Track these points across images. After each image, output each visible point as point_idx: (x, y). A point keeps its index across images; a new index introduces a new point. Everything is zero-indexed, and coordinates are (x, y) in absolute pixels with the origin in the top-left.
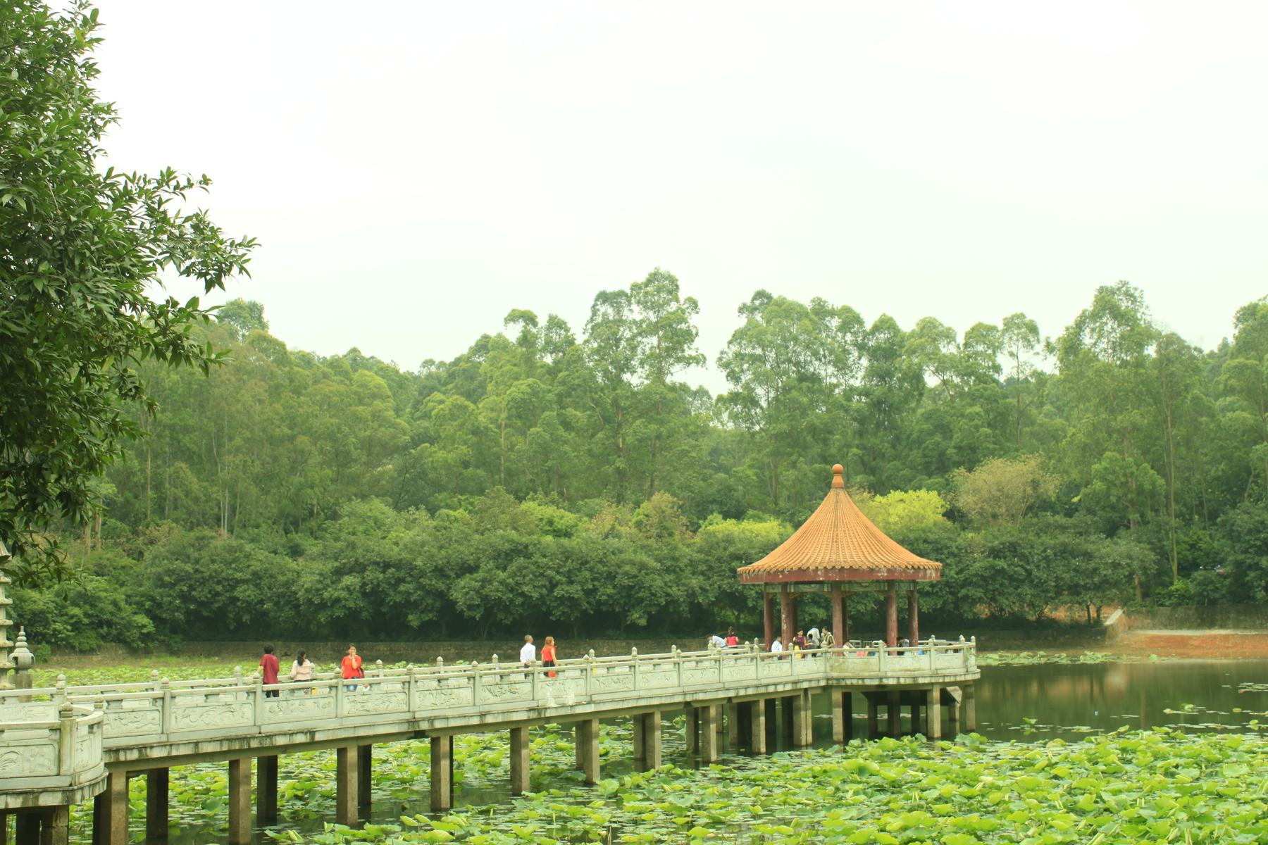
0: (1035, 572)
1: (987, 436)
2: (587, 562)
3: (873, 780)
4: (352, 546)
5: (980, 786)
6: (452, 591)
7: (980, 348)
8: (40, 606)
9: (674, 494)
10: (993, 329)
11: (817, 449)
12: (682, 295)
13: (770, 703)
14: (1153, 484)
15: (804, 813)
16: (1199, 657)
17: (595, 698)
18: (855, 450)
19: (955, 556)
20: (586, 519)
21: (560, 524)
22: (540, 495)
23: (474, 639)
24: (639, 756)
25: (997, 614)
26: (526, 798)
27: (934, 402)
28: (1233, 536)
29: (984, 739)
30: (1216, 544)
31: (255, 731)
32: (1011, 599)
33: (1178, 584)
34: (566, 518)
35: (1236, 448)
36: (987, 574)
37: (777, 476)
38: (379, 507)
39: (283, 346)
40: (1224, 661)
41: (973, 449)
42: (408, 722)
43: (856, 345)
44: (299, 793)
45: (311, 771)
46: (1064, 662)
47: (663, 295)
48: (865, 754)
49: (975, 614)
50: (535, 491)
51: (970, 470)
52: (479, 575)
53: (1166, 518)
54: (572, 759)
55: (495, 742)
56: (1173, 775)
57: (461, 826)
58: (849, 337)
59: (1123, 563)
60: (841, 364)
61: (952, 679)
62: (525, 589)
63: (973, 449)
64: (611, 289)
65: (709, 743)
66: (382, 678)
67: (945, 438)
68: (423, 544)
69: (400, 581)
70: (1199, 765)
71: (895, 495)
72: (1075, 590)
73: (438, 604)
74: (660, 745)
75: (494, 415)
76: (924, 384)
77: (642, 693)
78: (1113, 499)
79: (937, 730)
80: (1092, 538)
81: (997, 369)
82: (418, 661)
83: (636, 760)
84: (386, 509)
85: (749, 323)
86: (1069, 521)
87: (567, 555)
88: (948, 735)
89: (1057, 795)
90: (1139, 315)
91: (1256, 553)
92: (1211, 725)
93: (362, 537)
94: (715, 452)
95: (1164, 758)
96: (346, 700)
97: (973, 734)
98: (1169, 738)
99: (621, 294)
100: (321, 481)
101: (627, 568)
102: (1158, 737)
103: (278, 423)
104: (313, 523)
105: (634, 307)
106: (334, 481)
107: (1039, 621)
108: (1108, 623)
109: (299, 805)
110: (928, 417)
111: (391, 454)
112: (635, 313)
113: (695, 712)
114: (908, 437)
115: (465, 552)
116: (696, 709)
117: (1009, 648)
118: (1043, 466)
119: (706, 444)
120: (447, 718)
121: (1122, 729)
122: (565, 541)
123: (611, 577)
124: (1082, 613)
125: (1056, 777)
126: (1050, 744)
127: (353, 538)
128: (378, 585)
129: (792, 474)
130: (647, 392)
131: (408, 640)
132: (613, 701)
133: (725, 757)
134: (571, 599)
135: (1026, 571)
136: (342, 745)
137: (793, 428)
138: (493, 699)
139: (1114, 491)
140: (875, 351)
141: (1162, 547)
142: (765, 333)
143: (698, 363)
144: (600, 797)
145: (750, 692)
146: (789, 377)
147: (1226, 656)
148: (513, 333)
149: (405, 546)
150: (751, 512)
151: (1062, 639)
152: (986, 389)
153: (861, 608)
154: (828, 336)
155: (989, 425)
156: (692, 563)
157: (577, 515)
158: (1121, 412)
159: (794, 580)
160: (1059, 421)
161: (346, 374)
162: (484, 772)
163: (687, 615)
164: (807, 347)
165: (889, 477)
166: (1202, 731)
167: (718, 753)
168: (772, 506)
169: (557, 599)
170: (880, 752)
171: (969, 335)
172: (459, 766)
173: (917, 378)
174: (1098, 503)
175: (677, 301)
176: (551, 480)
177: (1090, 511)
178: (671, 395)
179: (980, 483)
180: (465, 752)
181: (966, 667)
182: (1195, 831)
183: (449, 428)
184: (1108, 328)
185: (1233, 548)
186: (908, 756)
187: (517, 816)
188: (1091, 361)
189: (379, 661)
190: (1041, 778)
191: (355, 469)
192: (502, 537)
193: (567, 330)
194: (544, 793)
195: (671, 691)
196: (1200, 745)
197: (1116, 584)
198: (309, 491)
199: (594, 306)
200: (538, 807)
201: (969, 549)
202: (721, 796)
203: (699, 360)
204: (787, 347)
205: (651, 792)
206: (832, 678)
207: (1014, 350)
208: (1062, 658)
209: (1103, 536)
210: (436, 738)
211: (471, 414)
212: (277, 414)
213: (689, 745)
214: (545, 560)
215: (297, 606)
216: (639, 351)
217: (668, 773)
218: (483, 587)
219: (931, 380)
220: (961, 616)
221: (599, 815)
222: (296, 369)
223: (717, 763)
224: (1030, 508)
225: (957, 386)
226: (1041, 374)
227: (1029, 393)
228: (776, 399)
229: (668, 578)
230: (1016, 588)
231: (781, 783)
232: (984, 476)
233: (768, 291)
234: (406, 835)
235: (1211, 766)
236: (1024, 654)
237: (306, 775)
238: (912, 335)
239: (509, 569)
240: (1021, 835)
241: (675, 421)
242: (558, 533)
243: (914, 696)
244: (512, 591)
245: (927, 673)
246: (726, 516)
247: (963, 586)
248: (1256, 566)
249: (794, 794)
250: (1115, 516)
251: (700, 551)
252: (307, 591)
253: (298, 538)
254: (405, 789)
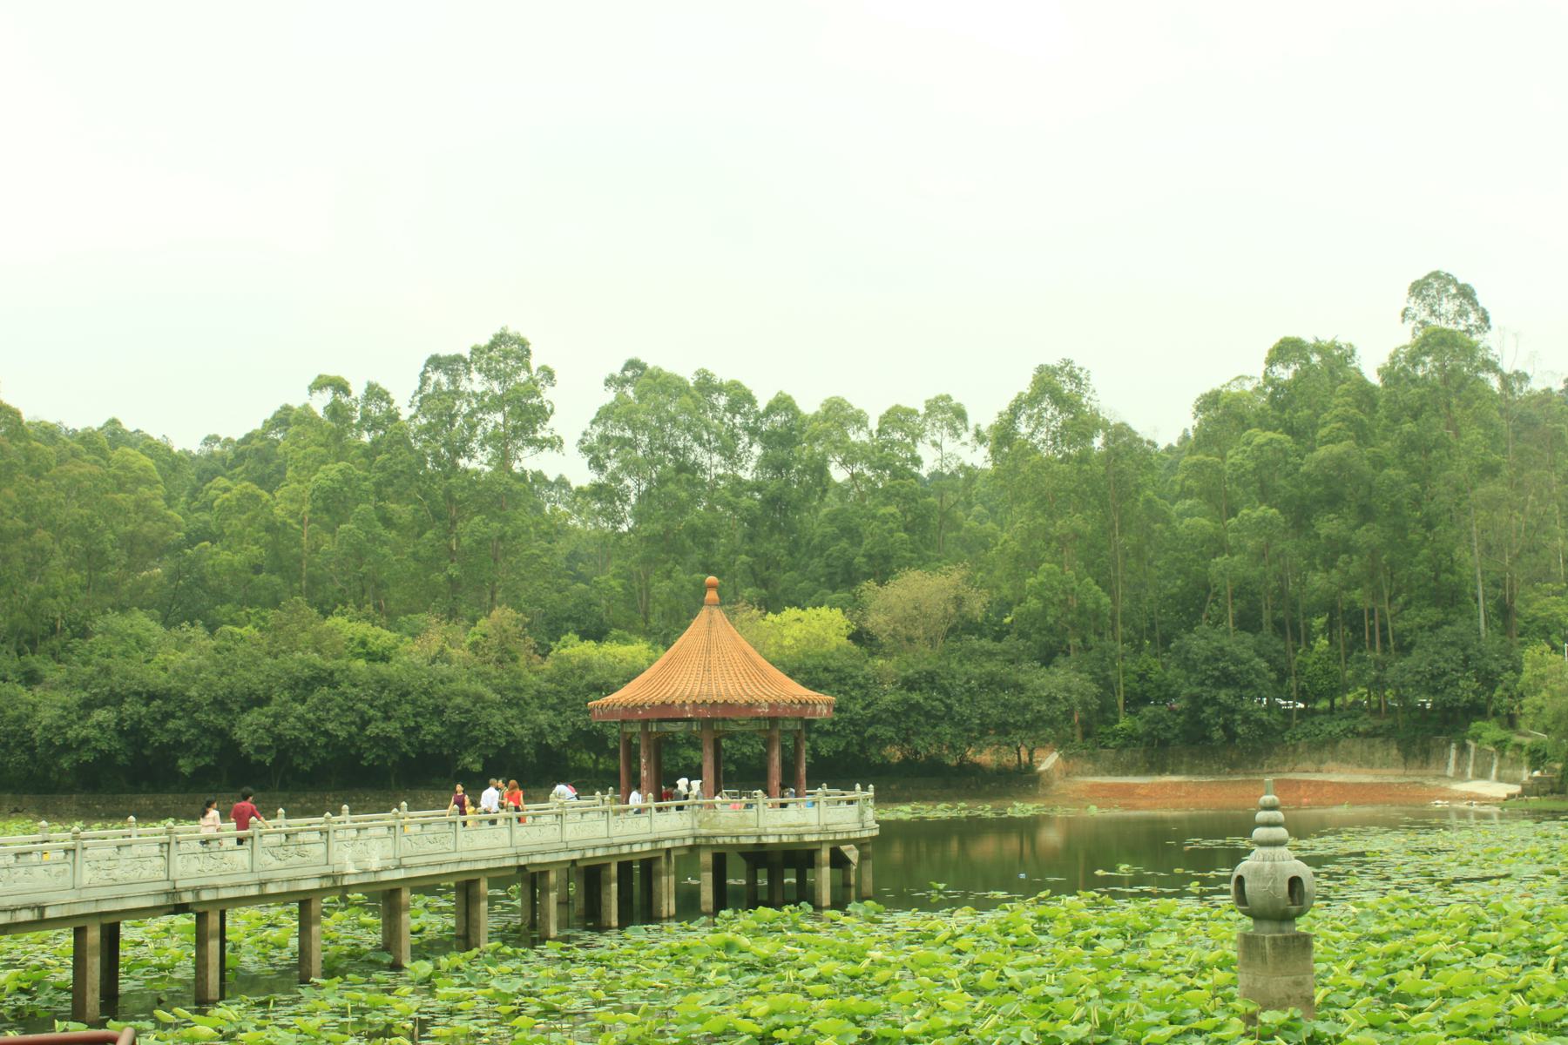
0: (956, 707)
1: (903, 542)
2: (409, 693)
3: (742, 958)
4: (106, 671)
5: (866, 962)
6: (236, 729)
7: (897, 436)
9: (519, 609)
10: (913, 412)
11: (697, 556)
12: (535, 362)
13: (625, 867)
14: (1097, 602)
15: (656, 997)
16: (1146, 808)
17: (405, 861)
18: (743, 557)
19: (861, 687)
20: (408, 639)
21: (375, 645)
22: (351, 609)
23: (262, 789)
24: (461, 933)
25: (912, 758)
26: (317, 986)
27: (842, 500)
28: (1188, 664)
29: (881, 908)
30: (1169, 675)
32: (928, 739)
33: (1124, 723)
34: (383, 637)
35: (1193, 560)
36: (899, 709)
37: (648, 590)
38: (142, 622)
39: (16, 414)
40: (1176, 813)
41: (887, 558)
42: (167, 893)
43: (746, 428)
44: (25, 985)
45: (43, 958)
46: (989, 815)
47: (511, 362)
48: (737, 927)
49: (884, 757)
50: (345, 604)
51: (881, 583)
52: (271, 709)
53: (1111, 643)
54: (377, 938)
55: (282, 917)
56: (1092, 947)
57: (231, 1022)
58: (738, 420)
59: (1060, 696)
60: (728, 451)
61: (845, 836)
62: (330, 726)
63: (887, 558)
64: (445, 352)
65: (547, 916)
66: (134, 838)
67: (853, 544)
68: (199, 670)
69: (169, 716)
70: (1124, 936)
71: (791, 613)
72: (1003, 729)
73: (217, 745)
74: (487, 921)
75: (295, 507)
76: (829, 478)
77: (465, 856)
78: (1050, 620)
79: (826, 897)
80: (1025, 666)
81: (917, 461)
82: (179, 816)
83: (458, 937)
84: (152, 624)
85: (617, 399)
86: (998, 646)
87: (383, 684)
88: (839, 904)
89: (953, 974)
90: (1084, 401)
91: (1214, 685)
92: (1146, 889)
93: (120, 660)
94: (573, 557)
95: (1085, 927)
96: (86, 866)
97: (869, 903)
98: (1096, 905)
99: (458, 359)
100: (67, 588)
101: (459, 700)
102: (1082, 904)
103: (10, 513)
104: (55, 642)
105: (475, 375)
106: (83, 588)
107: (960, 765)
108: (1042, 768)
109: (23, 1000)
110: (832, 518)
111: (161, 554)
112: (475, 383)
113: (531, 878)
114: (808, 543)
115: (254, 680)
116: (534, 874)
117: (924, 799)
118: (968, 580)
119: (562, 547)
120: (217, 888)
121: (1042, 894)
122: (380, 667)
123: (438, 711)
124: (1010, 757)
125: (959, 952)
126: (958, 912)
127: (107, 661)
128: (140, 722)
129: (666, 585)
130: (491, 482)
131: (178, 791)
132: (428, 865)
133: (568, 932)
134: (388, 739)
135: (947, 706)
136: (80, 924)
137: (668, 530)
138: (277, 864)
139: (1052, 611)
140: (769, 437)
141: (1106, 678)
142: (636, 411)
143: (552, 447)
144: (408, 983)
145: (599, 853)
146: (665, 467)
147: (1176, 807)
148: (320, 403)
149: (176, 671)
150: (615, 632)
151: (987, 788)
152: (903, 486)
153: (747, 750)
154: (714, 417)
155: (906, 529)
156: (539, 695)
157: (397, 635)
158: (1061, 517)
159: (656, 716)
160: (989, 525)
161: (101, 452)
162: (265, 956)
163: (532, 759)
164: (689, 430)
165: (785, 591)
166: (1133, 895)
167: (559, 928)
168: (641, 625)
169: (369, 738)
170: (755, 924)
171: (884, 420)
172: (234, 949)
173: (820, 470)
174: (1033, 624)
175: (529, 370)
176: (367, 590)
177: (1023, 635)
178: (518, 487)
179: (893, 600)
180: (243, 929)
181: (862, 821)
182: (1103, 1010)
183: (236, 523)
184: (1048, 415)
185: (1187, 679)
186: (789, 929)
187: (303, 1007)
188: (1027, 453)
189: (132, 818)
190: (941, 954)
191: (112, 573)
192: (301, 661)
193: (390, 402)
194: (339, 979)
195: (501, 852)
196: (1129, 911)
197: (1051, 722)
198: (51, 601)
199: (423, 374)
200: (327, 997)
201: (878, 679)
202: (558, 979)
203: (554, 443)
204: (663, 430)
205: (472, 976)
206: (701, 836)
207: (937, 438)
208: (986, 810)
209: (1037, 664)
210: (206, 915)
211: (265, 505)
212: (9, 502)
213: (524, 918)
214: (355, 690)
215: (32, 749)
216: (479, 430)
217: (496, 952)
218: (275, 724)
219: (838, 474)
220: (867, 759)
221: (405, 1003)
222: (35, 444)
223: (555, 939)
224: (952, 630)
225: (869, 480)
226: (973, 467)
227: (956, 491)
228: (648, 492)
229: (509, 713)
230: (934, 727)
231: (632, 962)
232: (899, 591)
233: (643, 360)
234: (160, 1033)
235: (1136, 936)
236: (942, 806)
237: (35, 963)
238: (816, 417)
239: (309, 702)
240: (907, 1018)
241: (524, 518)
242: (372, 657)
243: (798, 857)
244: (312, 729)
245: (815, 828)
246: (584, 636)
247: (870, 724)
248: (1213, 701)
249: (647, 976)
250: (1052, 640)
251: (550, 680)
252: (45, 728)
253: (34, 661)
254: (163, 977)
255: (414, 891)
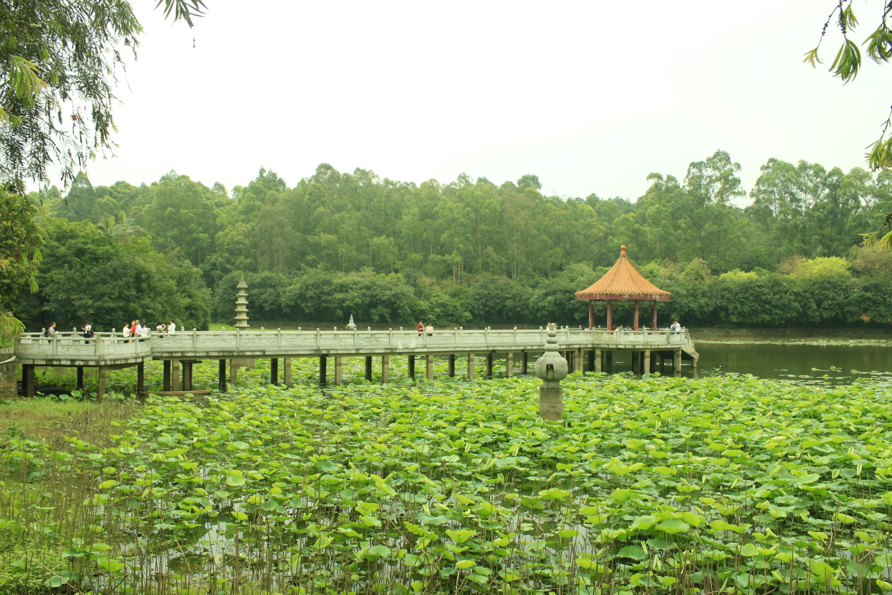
8: (423, 308)
12: (733, 161)
31: (236, 350)
64: (696, 161)
92: (887, 373)
112: (708, 172)
229: (690, 299)
255: (476, 355)
